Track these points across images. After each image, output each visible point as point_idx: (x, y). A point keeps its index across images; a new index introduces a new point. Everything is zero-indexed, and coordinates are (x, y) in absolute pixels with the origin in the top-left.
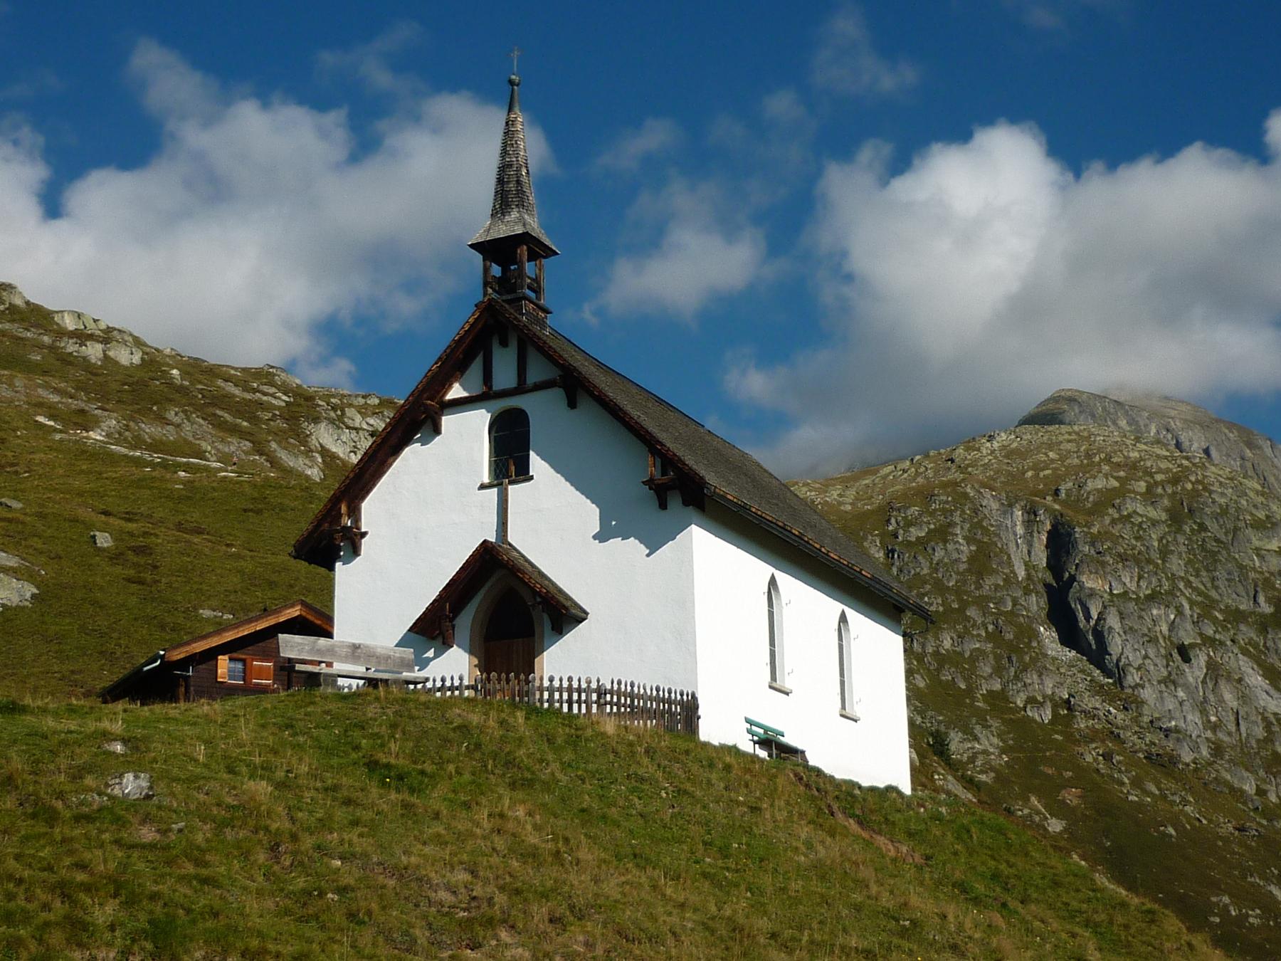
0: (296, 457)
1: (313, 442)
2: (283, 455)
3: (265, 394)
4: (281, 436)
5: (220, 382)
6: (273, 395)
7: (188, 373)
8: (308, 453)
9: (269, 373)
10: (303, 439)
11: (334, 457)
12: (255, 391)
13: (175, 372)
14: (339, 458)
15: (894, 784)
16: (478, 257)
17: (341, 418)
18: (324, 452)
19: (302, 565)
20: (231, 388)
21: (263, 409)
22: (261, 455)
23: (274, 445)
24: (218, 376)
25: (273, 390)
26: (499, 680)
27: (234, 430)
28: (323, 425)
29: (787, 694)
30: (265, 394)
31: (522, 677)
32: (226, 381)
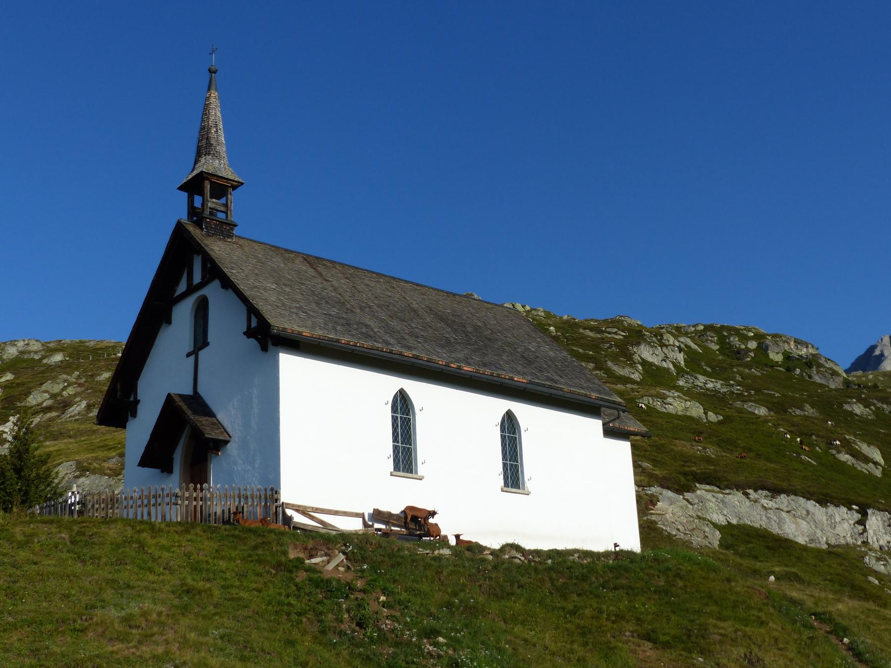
0: (623, 368)
1: (636, 358)
2: (615, 368)
3: (610, 333)
4: (615, 358)
5: (581, 330)
6: (615, 333)
7: (560, 328)
8: (633, 365)
9: (618, 321)
10: (629, 357)
11: (651, 364)
12: (605, 332)
13: (552, 328)
14: (655, 365)
15: (510, 541)
16: (184, 195)
17: (660, 340)
18: (644, 363)
19: (103, 428)
20: (588, 333)
21: (603, 343)
22: (600, 370)
23: (610, 363)
24: (580, 327)
25: (616, 330)
26: (195, 489)
27: (588, 359)
28: (642, 347)
29: (513, 477)
30: (610, 333)
31: (199, 486)
32: (585, 329)
